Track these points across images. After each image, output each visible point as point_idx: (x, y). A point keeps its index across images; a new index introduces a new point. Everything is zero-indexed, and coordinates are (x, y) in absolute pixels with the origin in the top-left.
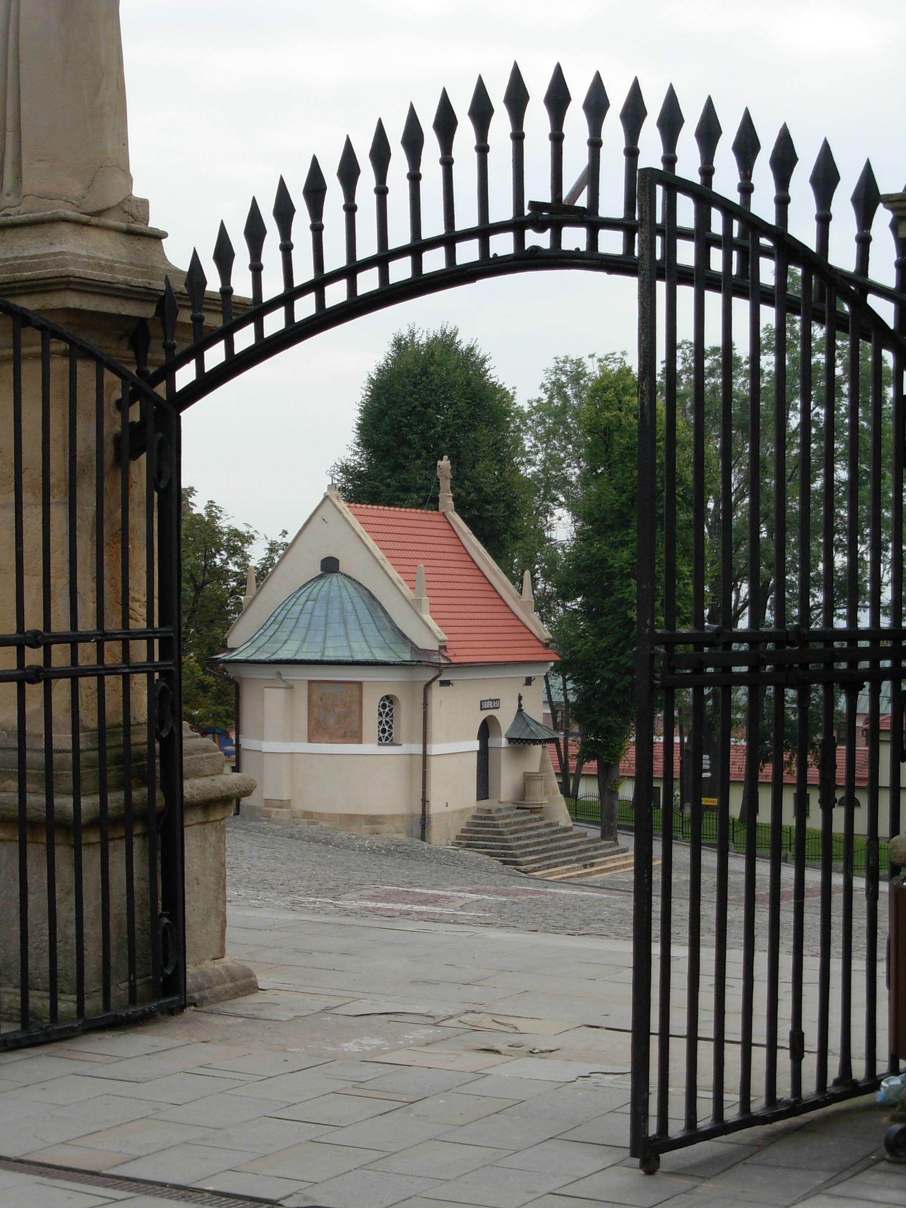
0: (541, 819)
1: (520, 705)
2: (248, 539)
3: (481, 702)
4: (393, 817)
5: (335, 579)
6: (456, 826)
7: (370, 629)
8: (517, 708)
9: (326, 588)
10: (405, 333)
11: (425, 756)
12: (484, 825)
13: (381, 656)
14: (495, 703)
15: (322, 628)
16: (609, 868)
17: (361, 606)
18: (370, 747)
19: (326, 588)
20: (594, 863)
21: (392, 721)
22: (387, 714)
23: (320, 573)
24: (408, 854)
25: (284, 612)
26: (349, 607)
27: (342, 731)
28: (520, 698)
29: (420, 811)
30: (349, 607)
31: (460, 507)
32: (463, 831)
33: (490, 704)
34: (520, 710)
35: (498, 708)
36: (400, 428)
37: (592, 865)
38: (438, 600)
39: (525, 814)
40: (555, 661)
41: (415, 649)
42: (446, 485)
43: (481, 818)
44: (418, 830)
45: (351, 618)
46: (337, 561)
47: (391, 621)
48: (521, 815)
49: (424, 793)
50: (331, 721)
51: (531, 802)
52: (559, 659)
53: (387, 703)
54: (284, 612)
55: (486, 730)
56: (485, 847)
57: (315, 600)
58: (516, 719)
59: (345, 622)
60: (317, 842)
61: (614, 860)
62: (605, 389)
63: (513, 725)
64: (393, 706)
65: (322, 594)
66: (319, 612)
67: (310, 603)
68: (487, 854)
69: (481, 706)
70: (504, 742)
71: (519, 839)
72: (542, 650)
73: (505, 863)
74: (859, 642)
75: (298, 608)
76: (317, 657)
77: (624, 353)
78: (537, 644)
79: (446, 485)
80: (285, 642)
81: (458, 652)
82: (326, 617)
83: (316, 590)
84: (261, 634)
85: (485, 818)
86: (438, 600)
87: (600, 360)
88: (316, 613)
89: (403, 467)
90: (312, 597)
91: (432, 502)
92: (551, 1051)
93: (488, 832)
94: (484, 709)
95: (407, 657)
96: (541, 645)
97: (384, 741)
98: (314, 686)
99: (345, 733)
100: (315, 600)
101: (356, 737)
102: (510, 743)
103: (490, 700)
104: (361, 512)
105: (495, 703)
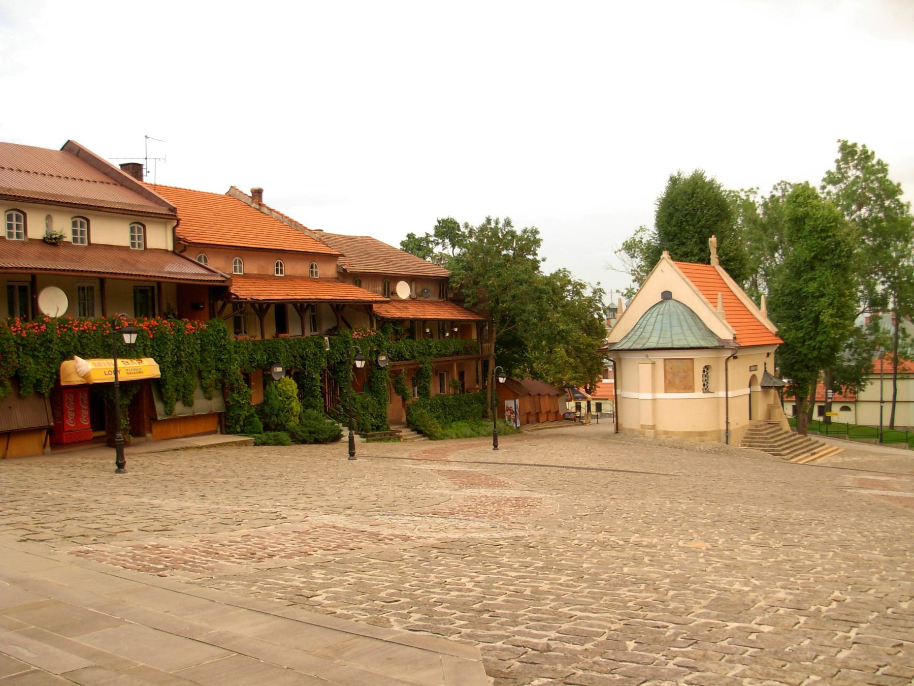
0: (781, 429)
2: (583, 286)
4: (711, 432)
5: (670, 302)
6: (742, 434)
7: (695, 329)
9: (667, 307)
10: (675, 174)
11: (727, 397)
12: (756, 434)
13: (703, 344)
15: (669, 329)
17: (688, 317)
18: (698, 394)
19: (667, 307)
23: (661, 300)
24: (717, 452)
25: (645, 322)
26: (682, 317)
28: (765, 364)
29: (725, 428)
30: (682, 317)
31: (721, 263)
32: (745, 438)
33: (753, 368)
34: (765, 371)
36: (682, 223)
37: (815, 453)
38: (729, 313)
39: (773, 427)
40: (780, 344)
41: (719, 340)
42: (713, 251)
43: (752, 430)
44: (724, 439)
45: (684, 324)
46: (671, 293)
47: (704, 325)
48: (770, 428)
49: (727, 418)
50: (677, 381)
51: (773, 420)
52: (782, 342)
54: (645, 322)
55: (752, 382)
56: (760, 446)
57: (662, 314)
58: (764, 375)
59: (681, 326)
60: (675, 447)
62: (798, 196)
63: (763, 379)
65: (666, 311)
66: (666, 321)
67: (659, 316)
68: (762, 450)
70: (759, 389)
71: (776, 441)
72: (774, 338)
73: (774, 455)
75: (652, 320)
76: (670, 346)
77: (758, 188)
78: (771, 335)
79: (713, 251)
80: (649, 338)
81: (742, 340)
82: (671, 323)
83: (662, 309)
84: (633, 335)
85: (756, 430)
86: (729, 313)
87: (746, 192)
88: (664, 321)
89: (684, 244)
90: (660, 313)
91: (709, 263)
92: (83, 536)
93: (760, 438)
95: (716, 344)
98: (667, 361)
100: (662, 314)
101: (690, 388)
104: (684, 266)
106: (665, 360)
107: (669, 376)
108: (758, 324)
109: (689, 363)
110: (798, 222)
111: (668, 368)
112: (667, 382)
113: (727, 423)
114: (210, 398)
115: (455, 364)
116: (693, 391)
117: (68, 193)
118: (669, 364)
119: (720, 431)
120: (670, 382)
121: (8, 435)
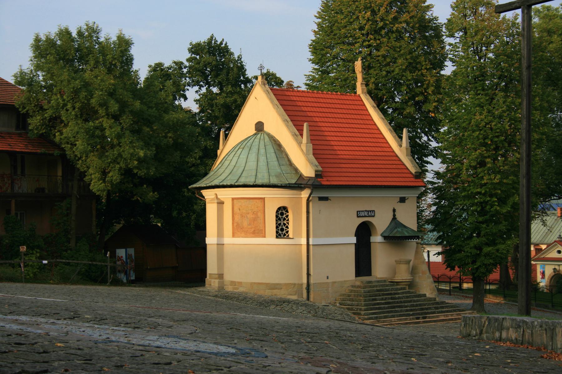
1: (394, 215)
3: (358, 212)
8: (392, 217)
14: (371, 213)
16: (440, 320)
20: (426, 317)
21: (288, 223)
22: (280, 224)
27: (253, 230)
28: (394, 210)
35: (374, 216)
53: (284, 212)
61: (452, 315)
64: (288, 214)
69: (358, 214)
72: (413, 179)
74: (472, 287)
78: (410, 175)
94: (360, 217)
96: (412, 176)
97: (282, 236)
99: (254, 231)
101: (261, 233)
102: (385, 239)
103: (366, 211)
105: (371, 213)
106: (233, 199)
107: (237, 218)
108: (399, 162)
109: (259, 203)
110: (127, 42)
111: (236, 209)
112: (235, 224)
113: (308, 275)
114: (453, 268)
115: (13, 202)
116: (264, 236)
117: (270, 106)
118: (237, 204)
119: (302, 285)
120: (238, 225)
121: (2, 264)
